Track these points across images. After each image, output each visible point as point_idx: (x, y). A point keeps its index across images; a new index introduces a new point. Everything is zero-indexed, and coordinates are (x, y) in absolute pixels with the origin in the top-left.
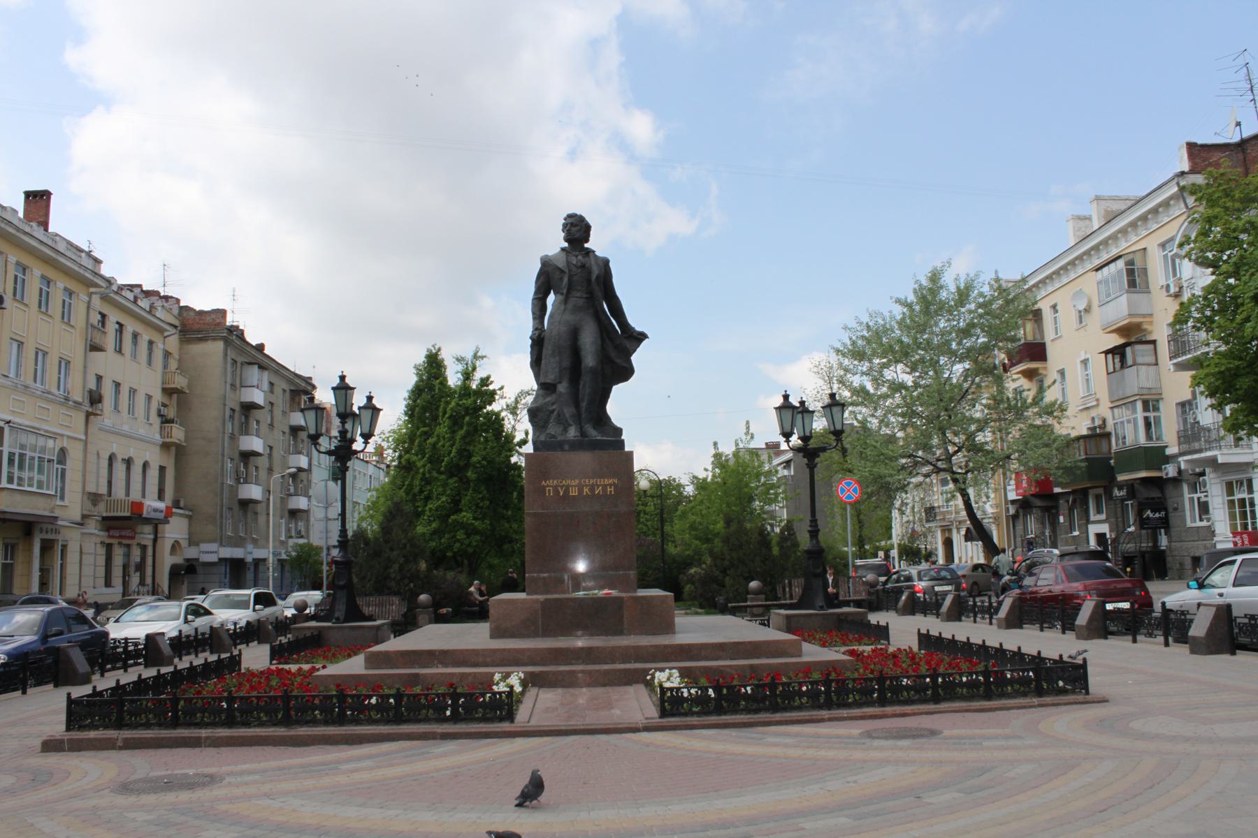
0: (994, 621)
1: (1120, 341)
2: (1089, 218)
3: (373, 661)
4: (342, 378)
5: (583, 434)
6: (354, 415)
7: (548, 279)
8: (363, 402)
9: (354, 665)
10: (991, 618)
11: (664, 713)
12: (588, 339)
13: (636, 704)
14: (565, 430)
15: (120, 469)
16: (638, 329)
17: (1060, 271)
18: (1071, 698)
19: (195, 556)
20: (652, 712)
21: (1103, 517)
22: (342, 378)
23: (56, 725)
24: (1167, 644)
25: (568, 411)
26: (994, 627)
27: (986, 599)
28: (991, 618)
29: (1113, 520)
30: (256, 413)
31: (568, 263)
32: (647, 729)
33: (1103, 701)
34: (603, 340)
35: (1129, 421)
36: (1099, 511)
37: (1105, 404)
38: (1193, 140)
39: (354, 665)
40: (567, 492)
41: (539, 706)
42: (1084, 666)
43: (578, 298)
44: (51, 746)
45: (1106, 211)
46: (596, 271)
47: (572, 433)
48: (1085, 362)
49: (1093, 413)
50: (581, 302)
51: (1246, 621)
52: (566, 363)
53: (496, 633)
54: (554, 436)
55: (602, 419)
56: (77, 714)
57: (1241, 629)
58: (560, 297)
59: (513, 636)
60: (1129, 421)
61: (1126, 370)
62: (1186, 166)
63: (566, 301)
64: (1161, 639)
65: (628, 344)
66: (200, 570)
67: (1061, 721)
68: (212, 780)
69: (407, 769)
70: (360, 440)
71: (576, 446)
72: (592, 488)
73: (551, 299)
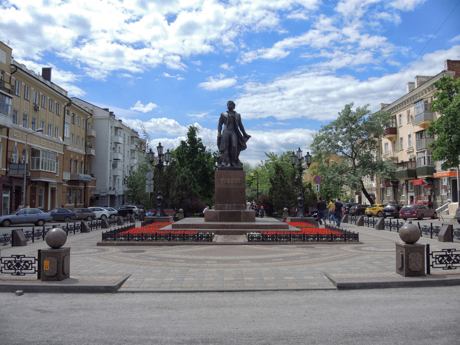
0: (375, 227)
1: (422, 129)
2: (414, 83)
3: (174, 226)
4: (160, 144)
5: (232, 165)
6: (163, 155)
7: (223, 120)
8: (166, 151)
9: (169, 227)
10: (374, 226)
11: (249, 241)
12: (234, 138)
13: (243, 239)
14: (227, 164)
15: (73, 162)
16: (248, 134)
17: (403, 103)
18: (353, 243)
19: (98, 194)
20: (247, 240)
21: (413, 190)
22: (160, 144)
23: (100, 239)
24: (432, 238)
25: (228, 159)
26: (375, 229)
27: (372, 218)
28: (374, 226)
29: (416, 191)
30: (119, 145)
31: (228, 116)
32: (245, 244)
33: (362, 243)
34: (238, 138)
35: (422, 157)
36: (412, 188)
37: (415, 151)
38: (449, 59)
39: (169, 227)
40: (227, 182)
41: (218, 238)
42: (358, 234)
43: (231, 126)
44: (99, 244)
45: (420, 81)
46: (237, 118)
47: (229, 165)
48: (410, 136)
49: (411, 154)
50: (232, 127)
51: (457, 231)
52: (228, 145)
53: (206, 220)
54: (223, 166)
55: (237, 161)
56: (105, 236)
57: (455, 233)
58: (226, 126)
59: (211, 221)
60: (422, 157)
61: (422, 139)
62: (446, 68)
63: (227, 127)
64: (430, 236)
65: (245, 139)
66: (100, 198)
67: (347, 248)
68: (143, 251)
69: (188, 250)
70: (165, 162)
71: (229, 169)
72: (234, 181)
73: (223, 125)
